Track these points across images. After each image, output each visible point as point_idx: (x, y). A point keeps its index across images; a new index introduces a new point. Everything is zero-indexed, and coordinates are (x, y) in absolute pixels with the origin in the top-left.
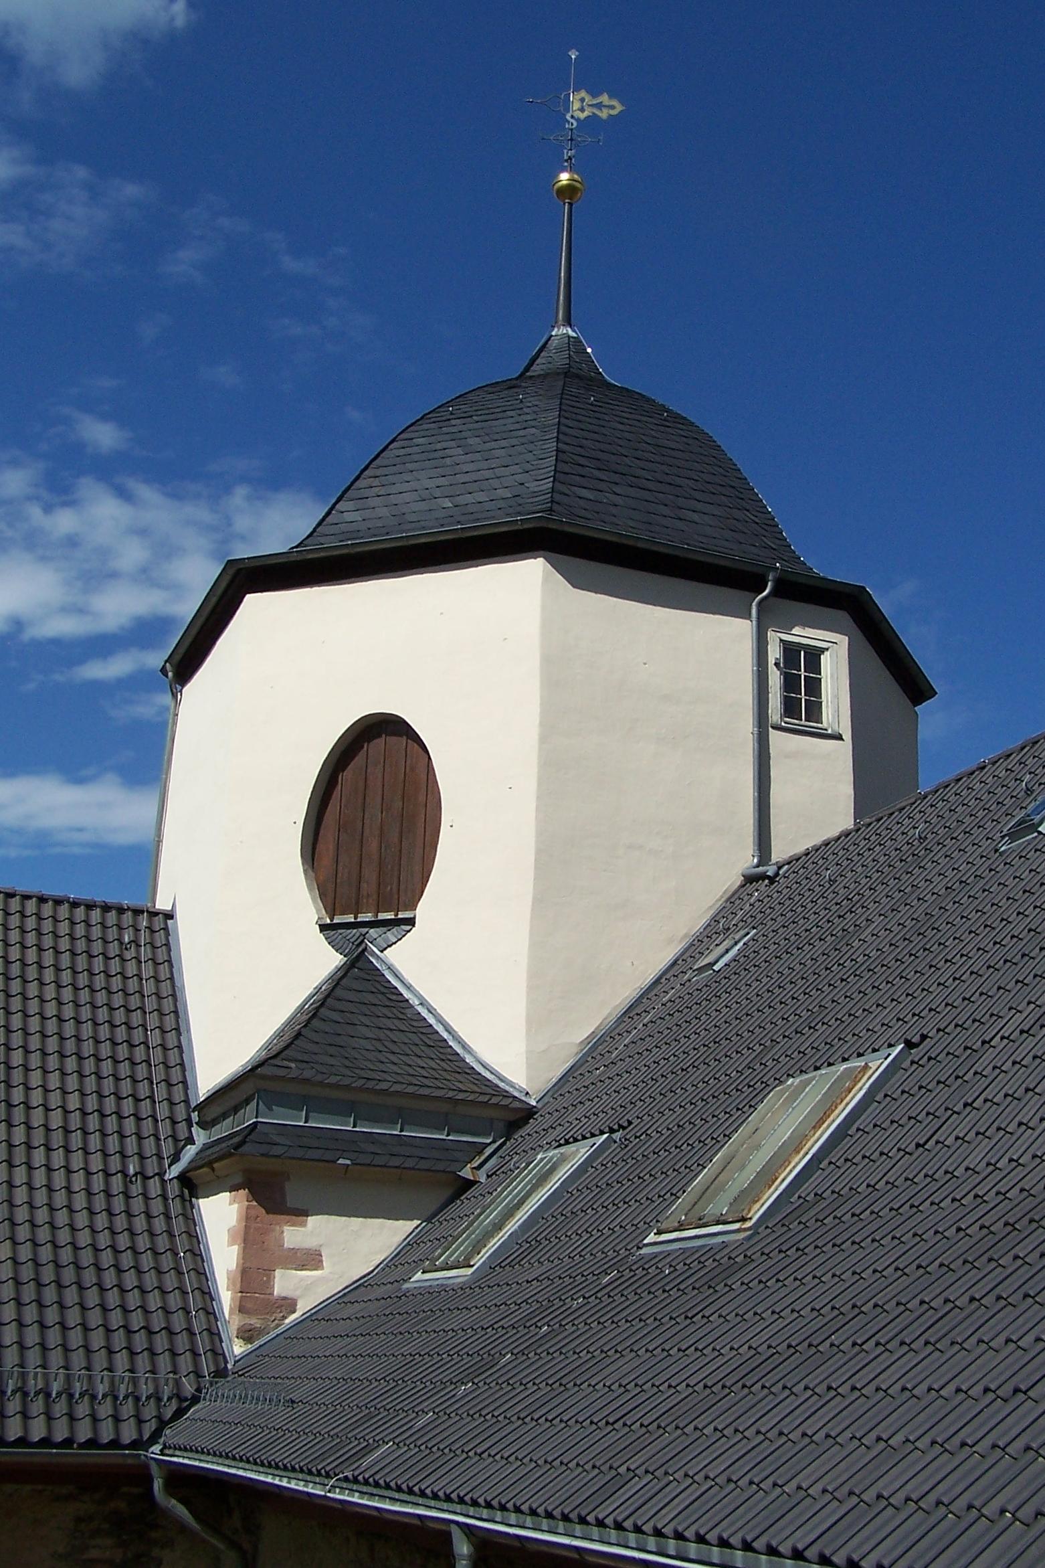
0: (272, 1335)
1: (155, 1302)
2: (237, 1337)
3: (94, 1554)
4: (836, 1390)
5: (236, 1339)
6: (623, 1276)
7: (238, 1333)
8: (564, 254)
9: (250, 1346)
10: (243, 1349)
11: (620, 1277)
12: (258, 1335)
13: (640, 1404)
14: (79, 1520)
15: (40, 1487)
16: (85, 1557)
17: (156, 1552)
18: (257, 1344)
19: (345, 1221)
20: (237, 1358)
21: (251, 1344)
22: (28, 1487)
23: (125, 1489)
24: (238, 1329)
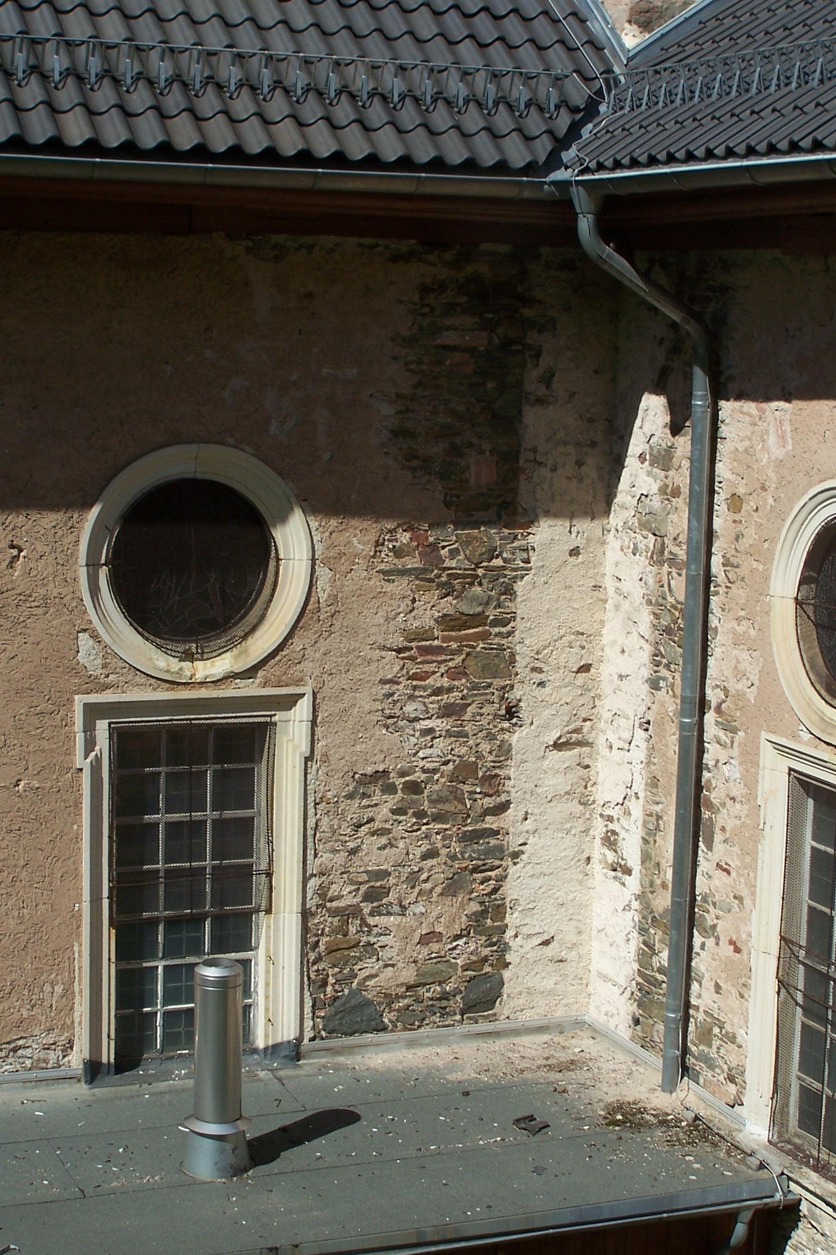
0: (679, 18)
1: (293, 566)
2: (630, 22)
3: (450, 338)
4: (663, 126)
5: (627, 25)
6: (792, 34)
7: (631, 15)
8: (206, 937)
9: (647, 36)
10: (637, 41)
11: (788, 36)
12: (660, 17)
13: (767, 125)
14: (425, 290)
15: (369, 241)
16: (439, 342)
17: (533, 337)
18: (658, 31)
19: (429, 156)
20: (631, 54)
21: (649, 33)
22: (353, 241)
23: (486, 247)
24: (631, 9)
